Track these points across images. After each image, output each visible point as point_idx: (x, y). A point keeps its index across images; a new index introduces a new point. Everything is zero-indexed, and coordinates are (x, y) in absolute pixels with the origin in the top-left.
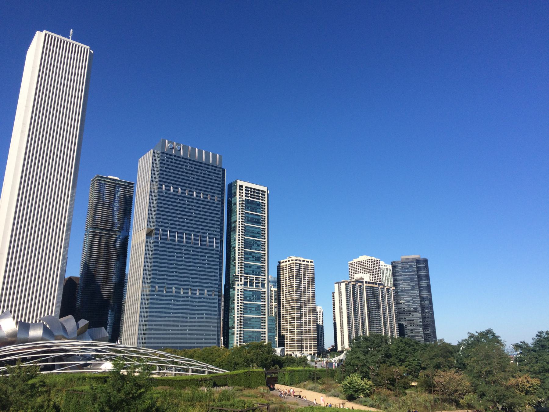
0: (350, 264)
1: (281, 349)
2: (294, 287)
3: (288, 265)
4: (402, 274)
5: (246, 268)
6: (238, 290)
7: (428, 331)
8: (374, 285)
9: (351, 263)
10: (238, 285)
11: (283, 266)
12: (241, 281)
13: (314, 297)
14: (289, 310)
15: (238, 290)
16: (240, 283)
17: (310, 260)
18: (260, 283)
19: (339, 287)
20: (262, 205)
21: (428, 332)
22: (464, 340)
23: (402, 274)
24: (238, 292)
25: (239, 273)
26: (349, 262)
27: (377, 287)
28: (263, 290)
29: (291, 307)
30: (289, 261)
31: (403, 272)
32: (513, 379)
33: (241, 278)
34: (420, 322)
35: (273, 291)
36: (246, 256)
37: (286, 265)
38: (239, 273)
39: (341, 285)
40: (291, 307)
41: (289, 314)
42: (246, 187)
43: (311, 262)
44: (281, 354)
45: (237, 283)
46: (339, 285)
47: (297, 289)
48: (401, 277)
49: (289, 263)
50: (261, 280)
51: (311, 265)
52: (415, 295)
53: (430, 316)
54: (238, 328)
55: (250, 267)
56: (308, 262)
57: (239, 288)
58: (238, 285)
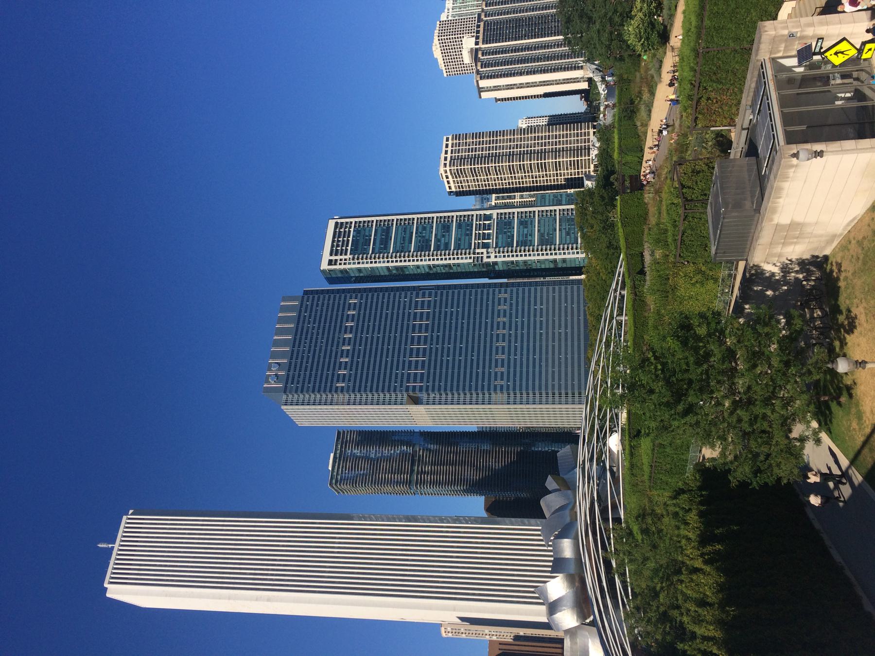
2: (488, 167)
3: (453, 178)
6: (496, 257)
8: (481, 29)
10: (489, 257)
11: (455, 186)
12: (482, 253)
14: (525, 173)
15: (496, 257)
16: (485, 255)
17: (445, 142)
19: (486, 91)
20: (359, 226)
24: (500, 257)
25: (470, 258)
27: (484, 24)
28: (495, 216)
29: (521, 169)
30: (447, 177)
33: (478, 253)
35: (496, 202)
36: (442, 247)
37: (454, 181)
38: (470, 258)
39: (482, 88)
40: (521, 169)
42: (331, 255)
43: (447, 140)
45: (485, 260)
46: (483, 91)
49: (450, 177)
50: (479, 240)
55: (460, 239)
56: (447, 146)
57: (493, 255)
58: (489, 257)
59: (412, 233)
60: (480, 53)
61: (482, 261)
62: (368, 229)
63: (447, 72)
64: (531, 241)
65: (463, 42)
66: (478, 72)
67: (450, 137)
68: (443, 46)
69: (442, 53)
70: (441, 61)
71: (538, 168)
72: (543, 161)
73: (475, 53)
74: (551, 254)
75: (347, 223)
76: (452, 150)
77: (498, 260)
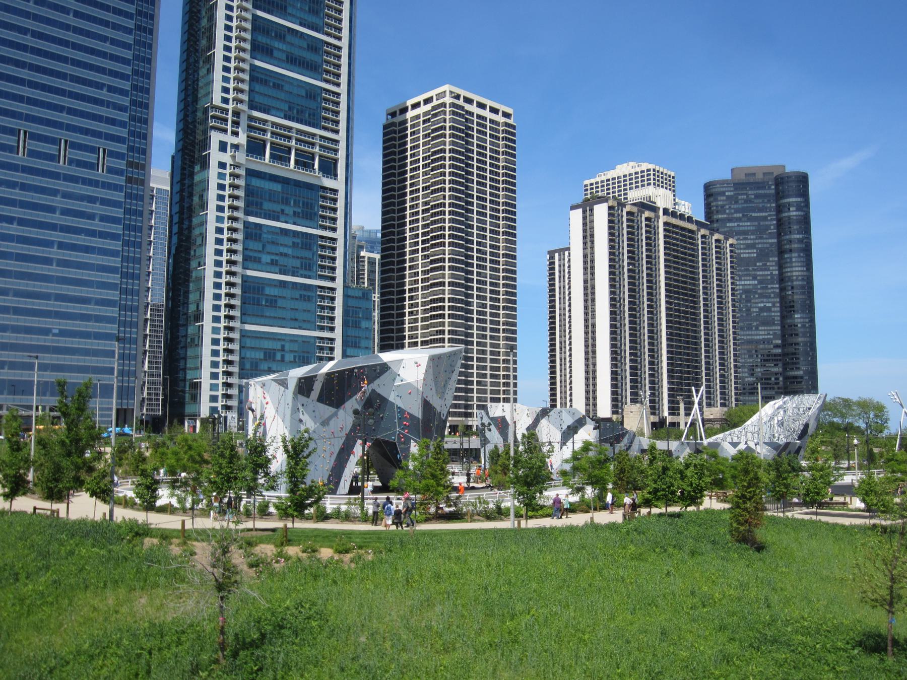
1: (433, 359)
3: (425, 114)
4: (735, 215)
5: (258, 87)
6: (222, 165)
7: (798, 369)
9: (592, 184)
12: (236, 134)
13: (511, 234)
14: (424, 272)
15: (222, 165)
16: (229, 139)
17: (502, 108)
19: (584, 218)
21: (800, 373)
24: (221, 176)
25: (225, 101)
26: (587, 182)
28: (328, 183)
29: (432, 262)
30: (427, 101)
32: (548, 449)
34: (776, 346)
35: (366, 259)
36: (262, 39)
37: (418, 117)
38: (225, 101)
39: (592, 210)
40: (432, 262)
41: (423, 288)
43: (506, 115)
44: (442, 405)
45: (216, 138)
46: (584, 212)
47: (457, 198)
49: (429, 107)
51: (507, 124)
52: (766, 273)
53: (802, 330)
54: (216, 319)
55: (277, 87)
56: (495, 111)
57: (226, 158)
58: (223, 147)
61: (213, 128)
64: (258, 260)
65: (668, 191)
66: (622, 205)
67: (511, 121)
70: (611, 174)
71: (432, 301)
72: (447, 312)
73: (647, 206)
74: (217, 308)
77: (213, 170)
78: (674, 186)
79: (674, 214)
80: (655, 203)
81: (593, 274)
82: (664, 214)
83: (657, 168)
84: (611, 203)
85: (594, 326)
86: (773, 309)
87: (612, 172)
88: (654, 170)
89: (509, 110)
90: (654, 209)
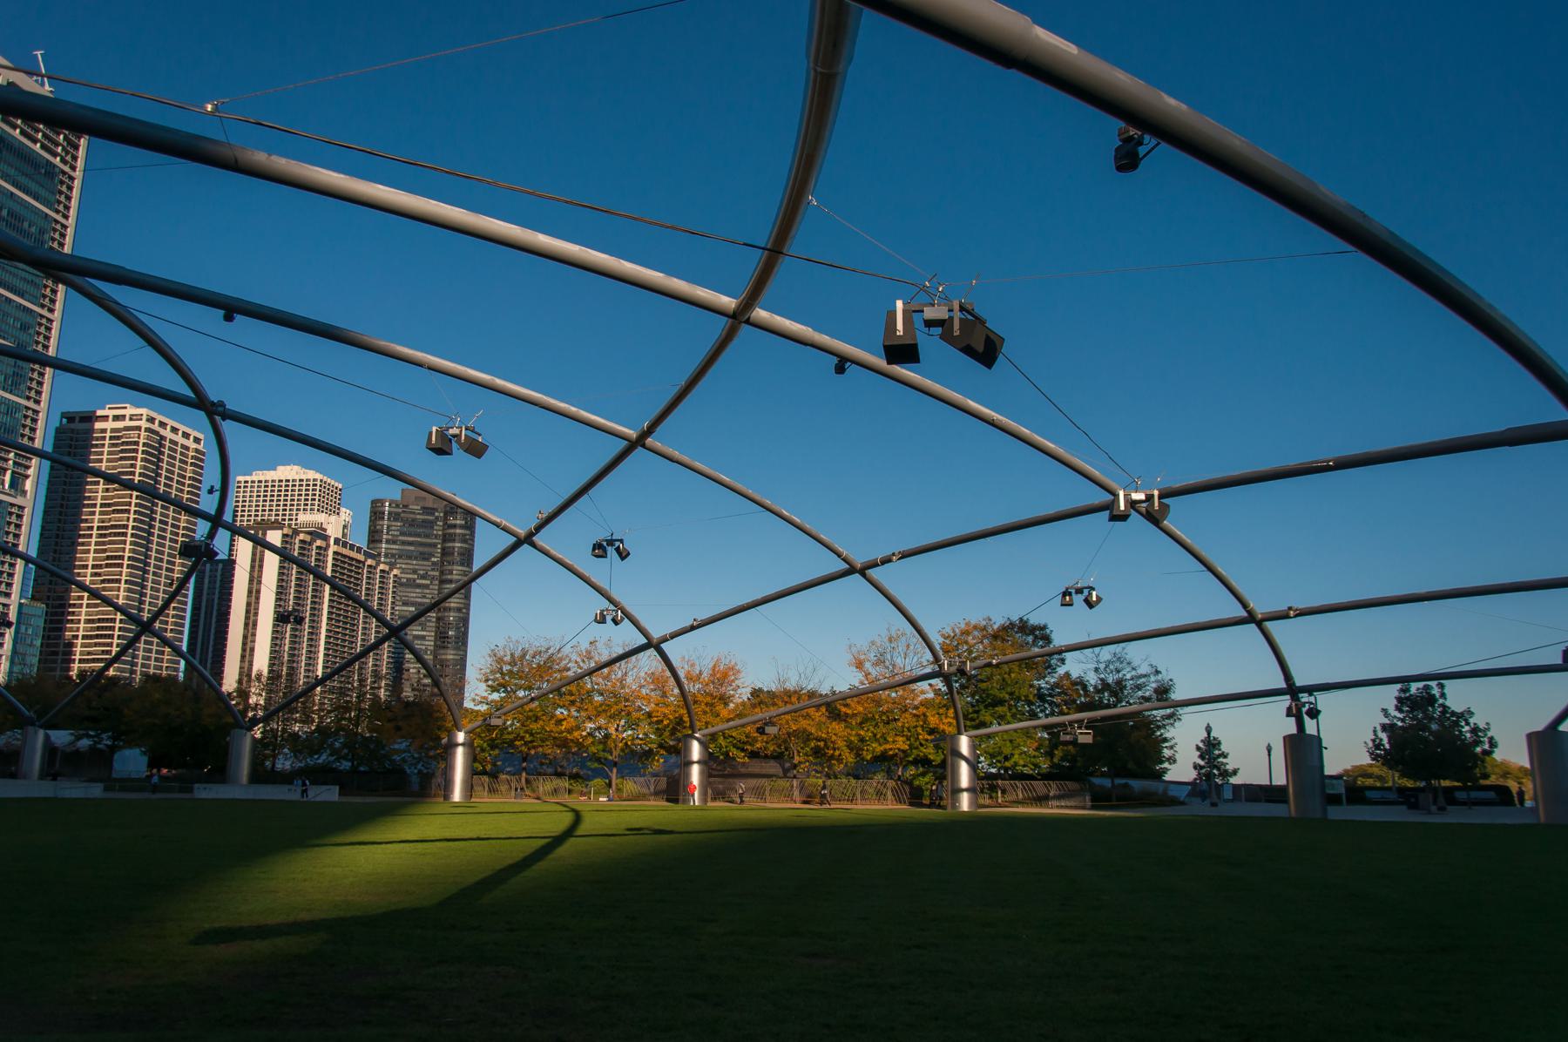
0: (242, 485)
2: (128, 511)
3: (113, 430)
4: (400, 538)
8: (353, 554)
11: (104, 431)
18: (9, 473)
20: (62, 183)
22: (975, 627)
23: (400, 538)
27: (359, 561)
28: (19, 501)
31: (402, 534)
43: (197, 440)
48: (394, 547)
49: (120, 425)
50: (15, 463)
51: (197, 451)
56: (186, 435)
59: (22, 296)
60: (323, 544)
62: (52, 198)
63: (246, 482)
66: (296, 532)
67: (200, 447)
68: (308, 485)
69: (288, 481)
75: (75, 158)
76: (175, 443)
78: (339, 499)
79: (345, 545)
80: (325, 530)
81: (258, 598)
82: (335, 544)
83: (325, 479)
84: (286, 531)
85: (252, 650)
86: (431, 587)
87: (272, 472)
88: (321, 481)
89: (200, 436)
90: (326, 538)
